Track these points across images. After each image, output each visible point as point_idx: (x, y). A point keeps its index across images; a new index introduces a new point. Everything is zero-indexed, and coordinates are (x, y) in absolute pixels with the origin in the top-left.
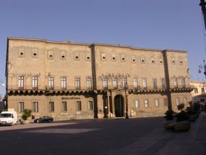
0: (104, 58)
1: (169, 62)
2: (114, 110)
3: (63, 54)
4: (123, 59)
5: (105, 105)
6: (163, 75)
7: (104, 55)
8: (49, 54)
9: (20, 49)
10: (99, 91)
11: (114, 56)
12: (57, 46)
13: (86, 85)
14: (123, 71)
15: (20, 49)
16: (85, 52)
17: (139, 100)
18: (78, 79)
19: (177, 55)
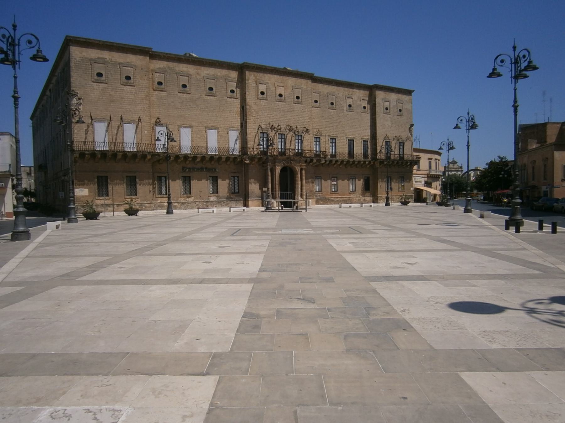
0: (262, 93)
1: (379, 110)
2: (278, 193)
3: (184, 80)
4: (298, 98)
5: (166, 190)
6: (367, 135)
7: (262, 88)
8: (157, 80)
9: (330, 97)
10: (252, 158)
11: (281, 90)
12: (171, 64)
13: (96, 140)
14: (299, 123)
15: (330, 97)
16: (227, 79)
17: (238, 177)
18: (333, 140)
19: (393, 97)
